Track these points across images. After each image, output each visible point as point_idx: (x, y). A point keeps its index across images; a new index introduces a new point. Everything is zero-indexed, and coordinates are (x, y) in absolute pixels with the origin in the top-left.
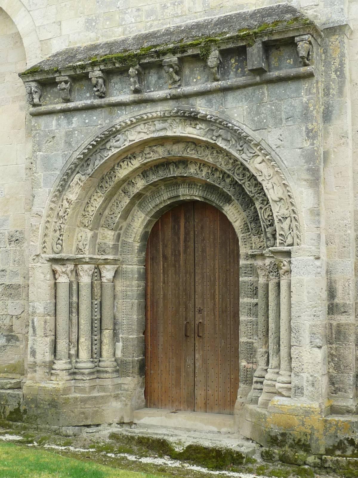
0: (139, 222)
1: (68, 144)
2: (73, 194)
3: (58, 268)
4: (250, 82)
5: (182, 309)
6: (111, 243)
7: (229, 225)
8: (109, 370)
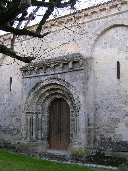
0: (47, 103)
1: (30, 85)
2: (31, 97)
3: (27, 114)
4: (69, 71)
5: (58, 125)
6: (41, 109)
7: (68, 104)
8: (40, 139)
